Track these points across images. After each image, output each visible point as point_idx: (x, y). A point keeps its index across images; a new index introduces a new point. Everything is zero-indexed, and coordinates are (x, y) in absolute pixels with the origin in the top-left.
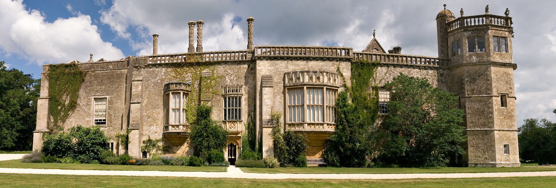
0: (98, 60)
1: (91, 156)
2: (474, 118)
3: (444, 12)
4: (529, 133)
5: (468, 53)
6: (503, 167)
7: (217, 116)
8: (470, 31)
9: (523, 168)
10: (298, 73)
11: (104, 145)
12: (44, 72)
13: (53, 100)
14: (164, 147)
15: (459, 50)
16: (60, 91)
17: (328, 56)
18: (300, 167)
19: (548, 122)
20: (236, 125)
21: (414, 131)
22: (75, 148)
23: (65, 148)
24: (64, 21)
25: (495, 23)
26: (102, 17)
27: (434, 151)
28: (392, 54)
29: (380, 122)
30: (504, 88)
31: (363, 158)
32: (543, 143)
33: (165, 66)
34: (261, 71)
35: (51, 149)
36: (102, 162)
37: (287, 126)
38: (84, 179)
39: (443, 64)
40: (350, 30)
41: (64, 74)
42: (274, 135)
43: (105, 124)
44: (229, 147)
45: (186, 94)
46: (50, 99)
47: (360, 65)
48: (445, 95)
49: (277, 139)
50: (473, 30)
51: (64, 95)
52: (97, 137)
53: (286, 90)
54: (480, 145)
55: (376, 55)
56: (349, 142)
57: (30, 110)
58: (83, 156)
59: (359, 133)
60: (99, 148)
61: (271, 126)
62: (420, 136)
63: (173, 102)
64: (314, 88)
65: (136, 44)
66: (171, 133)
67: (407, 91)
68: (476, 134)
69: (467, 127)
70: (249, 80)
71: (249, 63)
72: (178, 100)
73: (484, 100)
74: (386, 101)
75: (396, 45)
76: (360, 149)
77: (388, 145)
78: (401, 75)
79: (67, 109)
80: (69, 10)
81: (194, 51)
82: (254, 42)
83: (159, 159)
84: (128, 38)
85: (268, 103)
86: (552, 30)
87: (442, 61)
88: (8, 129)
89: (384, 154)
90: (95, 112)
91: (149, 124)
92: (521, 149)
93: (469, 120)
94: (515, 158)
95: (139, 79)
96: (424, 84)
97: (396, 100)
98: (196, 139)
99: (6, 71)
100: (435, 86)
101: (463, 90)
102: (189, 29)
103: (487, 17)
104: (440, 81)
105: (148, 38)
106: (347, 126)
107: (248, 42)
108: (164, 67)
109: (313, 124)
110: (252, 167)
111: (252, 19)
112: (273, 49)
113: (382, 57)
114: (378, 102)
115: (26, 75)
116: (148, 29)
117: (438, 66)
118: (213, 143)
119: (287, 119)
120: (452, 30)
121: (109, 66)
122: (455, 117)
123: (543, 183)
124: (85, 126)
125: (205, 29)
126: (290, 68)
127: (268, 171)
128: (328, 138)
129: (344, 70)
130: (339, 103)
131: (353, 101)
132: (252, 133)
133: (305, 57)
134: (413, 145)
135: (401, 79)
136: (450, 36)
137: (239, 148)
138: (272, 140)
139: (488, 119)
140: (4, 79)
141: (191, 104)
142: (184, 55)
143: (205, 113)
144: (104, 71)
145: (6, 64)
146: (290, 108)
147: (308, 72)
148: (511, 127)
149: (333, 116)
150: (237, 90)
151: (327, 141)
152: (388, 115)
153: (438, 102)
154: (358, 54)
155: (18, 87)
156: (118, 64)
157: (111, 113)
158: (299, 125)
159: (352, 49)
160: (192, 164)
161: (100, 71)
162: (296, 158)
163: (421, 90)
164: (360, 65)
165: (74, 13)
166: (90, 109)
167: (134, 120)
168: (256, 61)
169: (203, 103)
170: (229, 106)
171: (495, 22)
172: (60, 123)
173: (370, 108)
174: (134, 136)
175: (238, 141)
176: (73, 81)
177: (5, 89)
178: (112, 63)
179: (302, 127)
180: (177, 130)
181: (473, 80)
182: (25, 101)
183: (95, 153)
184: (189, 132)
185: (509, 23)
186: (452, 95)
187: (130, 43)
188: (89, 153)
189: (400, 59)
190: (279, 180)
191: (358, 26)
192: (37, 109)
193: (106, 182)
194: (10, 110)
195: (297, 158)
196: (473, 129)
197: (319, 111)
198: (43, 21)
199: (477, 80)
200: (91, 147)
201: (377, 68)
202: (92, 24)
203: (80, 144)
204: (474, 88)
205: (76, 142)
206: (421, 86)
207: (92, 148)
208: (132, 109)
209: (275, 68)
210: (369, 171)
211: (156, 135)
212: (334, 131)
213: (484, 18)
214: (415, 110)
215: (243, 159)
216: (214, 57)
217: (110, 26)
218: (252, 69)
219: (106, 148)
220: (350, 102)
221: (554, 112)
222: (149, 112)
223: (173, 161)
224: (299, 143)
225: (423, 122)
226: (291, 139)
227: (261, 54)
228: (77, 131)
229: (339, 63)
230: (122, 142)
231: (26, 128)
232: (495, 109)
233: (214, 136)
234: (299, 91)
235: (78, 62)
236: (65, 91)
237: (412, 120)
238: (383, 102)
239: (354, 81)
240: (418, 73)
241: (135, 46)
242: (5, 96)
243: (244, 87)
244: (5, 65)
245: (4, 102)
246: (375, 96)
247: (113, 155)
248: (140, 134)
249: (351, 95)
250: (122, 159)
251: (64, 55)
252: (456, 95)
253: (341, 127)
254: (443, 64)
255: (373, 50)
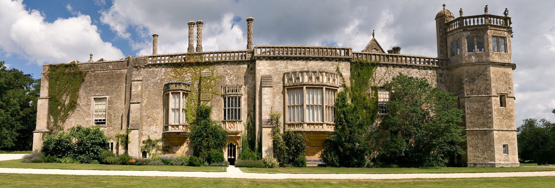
0: (98, 60)
1: (91, 156)
2: (473, 118)
3: (443, 12)
4: (528, 133)
5: (467, 53)
6: (503, 167)
7: (217, 116)
8: (469, 31)
9: (522, 168)
10: (298, 73)
11: (104, 145)
12: (44, 72)
13: (53, 100)
14: (164, 147)
15: (459, 50)
16: (60, 91)
17: (327, 56)
18: (300, 167)
19: (547, 122)
20: (236, 125)
21: (413, 131)
22: (75, 148)
23: (65, 148)
24: (64, 21)
25: (494, 23)
26: (102, 17)
27: (433, 151)
28: (391, 54)
29: (379, 122)
30: (504, 88)
31: (363, 158)
32: (542, 143)
33: (165, 66)
34: (260, 71)
35: (51, 149)
36: (102, 162)
37: (286, 126)
38: (84, 179)
39: (442, 64)
40: (349, 30)
41: (64, 74)
42: (274, 135)
43: (105, 124)
44: (228, 147)
45: (186, 94)
46: (50, 99)
47: (359, 65)
48: (444, 95)
49: (277, 139)
50: (472, 30)
51: (64, 95)
52: (97, 137)
53: (286, 90)
54: (479, 145)
55: (375, 55)
56: (349, 142)
57: (30, 110)
58: (83, 156)
59: (358, 133)
60: (99, 148)
61: (271, 126)
62: (419, 136)
63: (173, 102)
64: (313, 88)
65: (135, 44)
66: (171, 133)
67: (406, 91)
68: (475, 134)
69: (466, 127)
70: (249, 80)
71: (249, 63)
72: (177, 100)
73: (483, 100)
74: (385, 101)
75: (395, 45)
76: (359, 149)
77: (387, 145)
78: (400, 75)
79: (67, 109)
80: (69, 10)
81: (194, 51)
82: (253, 42)
83: (159, 159)
84: (128, 38)
85: (268, 103)
86: (551, 30)
87: (441, 61)
88: (8, 129)
89: (383, 154)
90: (95, 112)
91: (149, 124)
92: (520, 149)
93: (468, 120)
94: (514, 158)
95: (138, 79)
96: (423, 84)
97: (395, 100)
98: (196, 139)
99: (6, 71)
100: (434, 86)
101: (462, 90)
102: (189, 29)
103: (486, 17)
104: (439, 81)
105: (148, 38)
106: (346, 126)
107: (248, 42)
108: (163, 67)
109: (313, 124)
110: (251, 167)
111: (252, 19)
112: (273, 49)
113: (381, 57)
114: (377, 102)
115: (25, 75)
116: (148, 29)
117: (437, 66)
118: (213, 143)
119: (286, 119)
120: (451, 30)
121: (109, 66)
122: (455, 117)
123: (542, 183)
124: (85, 126)
125: (204, 29)
126: (289, 68)
127: (268, 171)
128: (328, 138)
129: (344, 70)
130: (338, 103)
131: (352, 101)
132: (251, 133)
133: (304, 57)
134: (413, 145)
135: (401, 79)
136: (450, 36)
137: (238, 148)
138: (272, 140)
139: (487, 119)
140: (4, 79)
141: (191, 104)
142: (183, 55)
143: (205, 113)
144: (104, 71)
145: (6, 64)
146: (290, 108)
147: (307, 72)
148: (510, 127)
149: (332, 116)
150: (236, 90)
151: (326, 141)
152: (387, 115)
153: (437, 102)
154: (357, 54)
155: (18, 87)
156: (118, 64)
157: (111, 113)
158: (298, 125)
159: (351, 49)
160: (191, 164)
161: (100, 71)
162: (296, 158)
163: (421, 90)
164: (359, 65)
165: (74, 13)
166: (89, 109)
167: (133, 120)
168: (255, 61)
169: (203, 103)
170: (229, 106)
171: (494, 22)
172: (60, 123)
173: (370, 108)
174: (134, 136)
175: (238, 141)
176: (73, 81)
177: (5, 89)
178: (112, 63)
179: (301, 127)
180: (177, 130)
181: (472, 80)
182: (25, 101)
183: (95, 153)
184: (188, 132)
185: (508, 23)
186: (451, 95)
187: (130, 43)
188: (89, 153)
189: (399, 59)
190: (279, 180)
191: (358, 26)
192: (37, 109)
193: (106, 182)
194: (10, 110)
195: (296, 158)
196: (472, 129)
197: (319, 111)
198: (43, 21)
199: (476, 80)
200: (91, 147)
201: (376, 68)
202: (92, 24)
203: (79, 144)
204: (473, 88)
205: (76, 142)
206: (420, 86)
207: (92, 148)
208: (131, 109)
209: (274, 68)
210: (368, 171)
211: (156, 135)
212: (333, 131)
213: (483, 18)
214: (414, 110)
215: (243, 159)
216: (214, 57)
217: (110, 26)
218: (251, 69)
219: (106, 148)
220: (349, 102)
221: (553, 112)
222: (149, 112)
223: (173, 161)
224: (299, 143)
225: (422, 122)
226: (291, 139)
227: (261, 54)
228: (77, 131)
229: (339, 63)
230: (122, 142)
231: (26, 128)
232: (494, 109)
233: (213, 136)
234: (298, 91)
235: (78, 62)
236: (65, 91)
237: (411, 120)
238: (382, 102)
239: (354, 81)
240: (417, 73)
241: (135, 46)
242: (5, 96)
243: (243, 87)
244: (5, 65)
245: (4, 102)
246: (374, 96)
247: (113, 155)
248: (139, 134)
249: (350, 95)
250: (121, 159)
251: (64, 55)
252: (455, 95)
253: (340, 127)
254: (442, 64)
255: (372, 50)
